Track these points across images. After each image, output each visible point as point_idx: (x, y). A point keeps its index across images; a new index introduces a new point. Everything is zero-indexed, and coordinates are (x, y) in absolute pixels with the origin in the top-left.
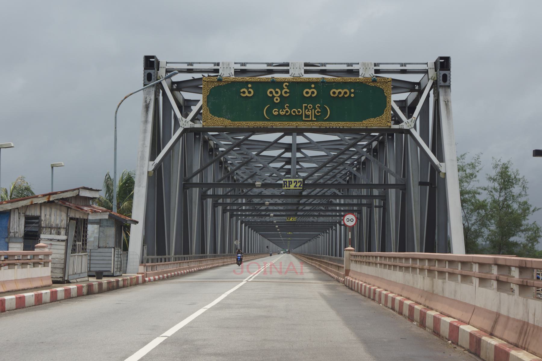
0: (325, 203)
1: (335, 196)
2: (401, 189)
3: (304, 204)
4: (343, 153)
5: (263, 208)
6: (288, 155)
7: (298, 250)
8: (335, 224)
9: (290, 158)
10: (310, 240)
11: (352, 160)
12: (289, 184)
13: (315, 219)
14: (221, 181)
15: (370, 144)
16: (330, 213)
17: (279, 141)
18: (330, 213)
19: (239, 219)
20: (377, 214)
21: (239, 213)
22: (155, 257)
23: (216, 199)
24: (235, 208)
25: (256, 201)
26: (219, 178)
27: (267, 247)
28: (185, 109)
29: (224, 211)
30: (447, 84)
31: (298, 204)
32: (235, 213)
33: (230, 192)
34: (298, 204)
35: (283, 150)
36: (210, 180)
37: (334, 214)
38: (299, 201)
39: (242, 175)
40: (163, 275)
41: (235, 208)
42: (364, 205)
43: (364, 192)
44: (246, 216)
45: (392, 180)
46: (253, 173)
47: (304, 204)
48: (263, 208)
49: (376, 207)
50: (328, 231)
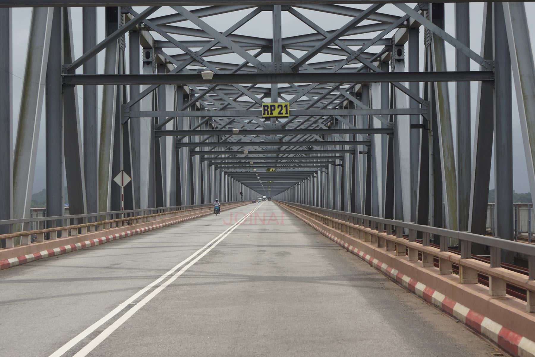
0: (306, 149)
2: (388, 134)
4: (324, 97)
5: (243, 156)
6: (267, 101)
7: (280, 196)
8: (312, 173)
10: (297, 183)
11: (334, 105)
12: (272, 110)
14: (206, 140)
15: (353, 87)
19: (223, 171)
20: (361, 159)
22: (155, 208)
23: (192, 147)
25: (235, 148)
26: (196, 125)
27: (241, 193)
28: (155, 51)
30: (401, 57)
31: (279, 151)
32: (213, 161)
33: (208, 139)
35: (263, 95)
36: (186, 128)
38: (279, 149)
39: (219, 122)
42: (347, 151)
43: (347, 137)
44: (228, 168)
45: (377, 124)
46: (230, 120)
47: (282, 158)
48: (243, 156)
49: (360, 153)
50: (308, 178)
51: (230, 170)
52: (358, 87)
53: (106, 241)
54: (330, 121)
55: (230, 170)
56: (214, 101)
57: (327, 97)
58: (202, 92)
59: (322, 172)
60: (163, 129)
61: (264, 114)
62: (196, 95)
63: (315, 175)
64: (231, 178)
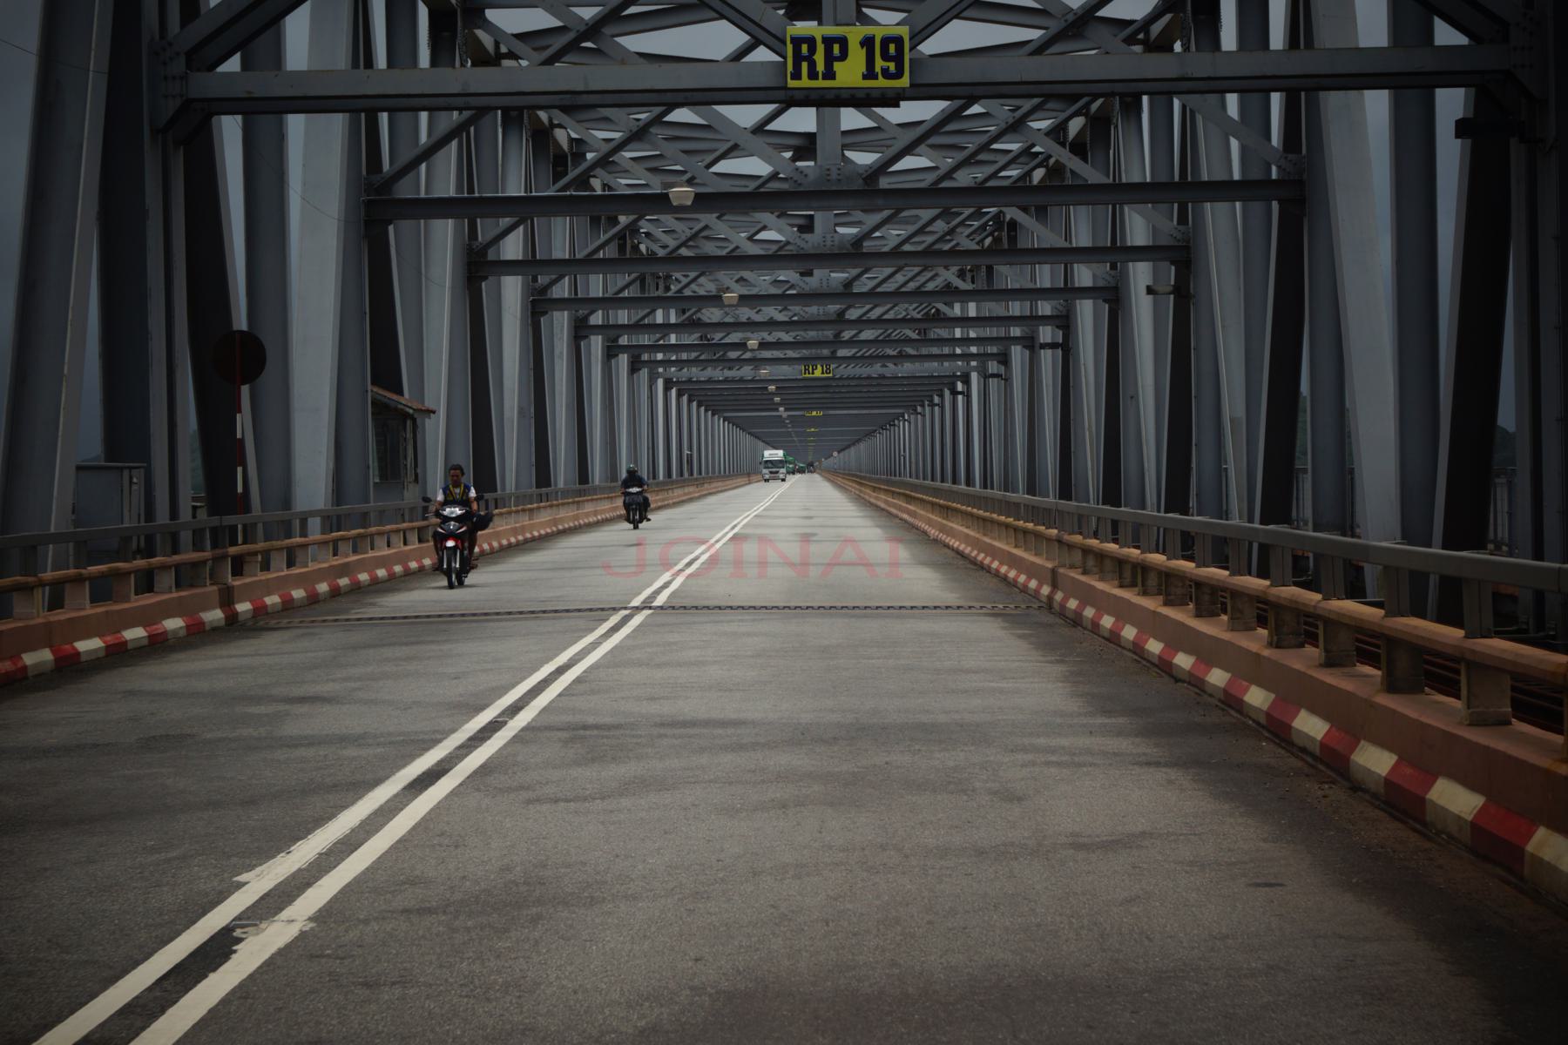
1: (949, 293)
2: (1172, 263)
3: (861, 322)
7: (858, 454)
9: (811, 137)
12: (830, 59)
13: (891, 369)
14: (622, 290)
16: (935, 350)
17: (768, 128)
18: (935, 350)
19: (659, 375)
20: (1143, 314)
21: (660, 356)
23: (542, 280)
24: (645, 339)
26: (620, 284)
29: (611, 352)
34: (846, 293)
36: (561, 251)
37: (946, 350)
38: (837, 335)
40: (371, 573)
41: (645, 339)
44: (680, 363)
47: (861, 322)
50: (919, 409)
51: (685, 373)
52: (1076, 125)
53: (280, 607)
54: (991, 234)
55: (685, 373)
56: (648, 174)
57: (981, 157)
58: (606, 148)
59: (985, 376)
60: (491, 256)
61: (797, 75)
62: (589, 156)
63: (960, 386)
64: (699, 406)
